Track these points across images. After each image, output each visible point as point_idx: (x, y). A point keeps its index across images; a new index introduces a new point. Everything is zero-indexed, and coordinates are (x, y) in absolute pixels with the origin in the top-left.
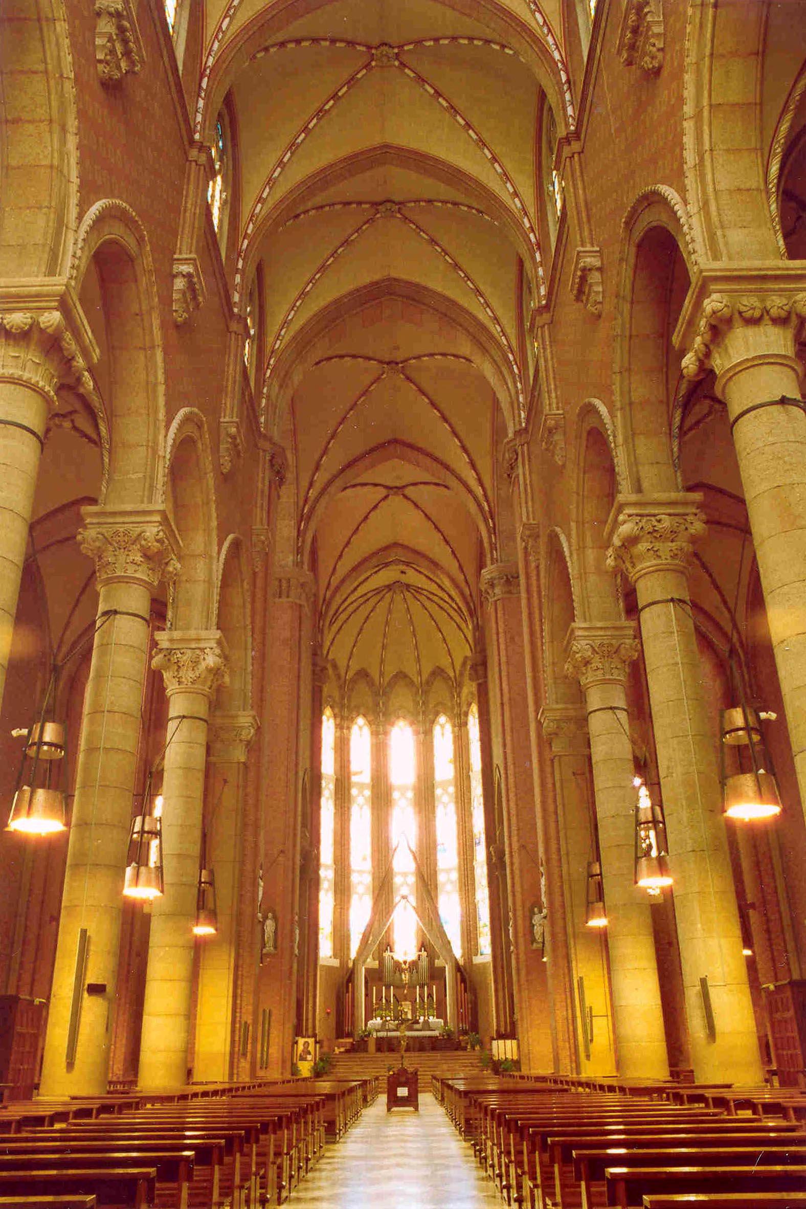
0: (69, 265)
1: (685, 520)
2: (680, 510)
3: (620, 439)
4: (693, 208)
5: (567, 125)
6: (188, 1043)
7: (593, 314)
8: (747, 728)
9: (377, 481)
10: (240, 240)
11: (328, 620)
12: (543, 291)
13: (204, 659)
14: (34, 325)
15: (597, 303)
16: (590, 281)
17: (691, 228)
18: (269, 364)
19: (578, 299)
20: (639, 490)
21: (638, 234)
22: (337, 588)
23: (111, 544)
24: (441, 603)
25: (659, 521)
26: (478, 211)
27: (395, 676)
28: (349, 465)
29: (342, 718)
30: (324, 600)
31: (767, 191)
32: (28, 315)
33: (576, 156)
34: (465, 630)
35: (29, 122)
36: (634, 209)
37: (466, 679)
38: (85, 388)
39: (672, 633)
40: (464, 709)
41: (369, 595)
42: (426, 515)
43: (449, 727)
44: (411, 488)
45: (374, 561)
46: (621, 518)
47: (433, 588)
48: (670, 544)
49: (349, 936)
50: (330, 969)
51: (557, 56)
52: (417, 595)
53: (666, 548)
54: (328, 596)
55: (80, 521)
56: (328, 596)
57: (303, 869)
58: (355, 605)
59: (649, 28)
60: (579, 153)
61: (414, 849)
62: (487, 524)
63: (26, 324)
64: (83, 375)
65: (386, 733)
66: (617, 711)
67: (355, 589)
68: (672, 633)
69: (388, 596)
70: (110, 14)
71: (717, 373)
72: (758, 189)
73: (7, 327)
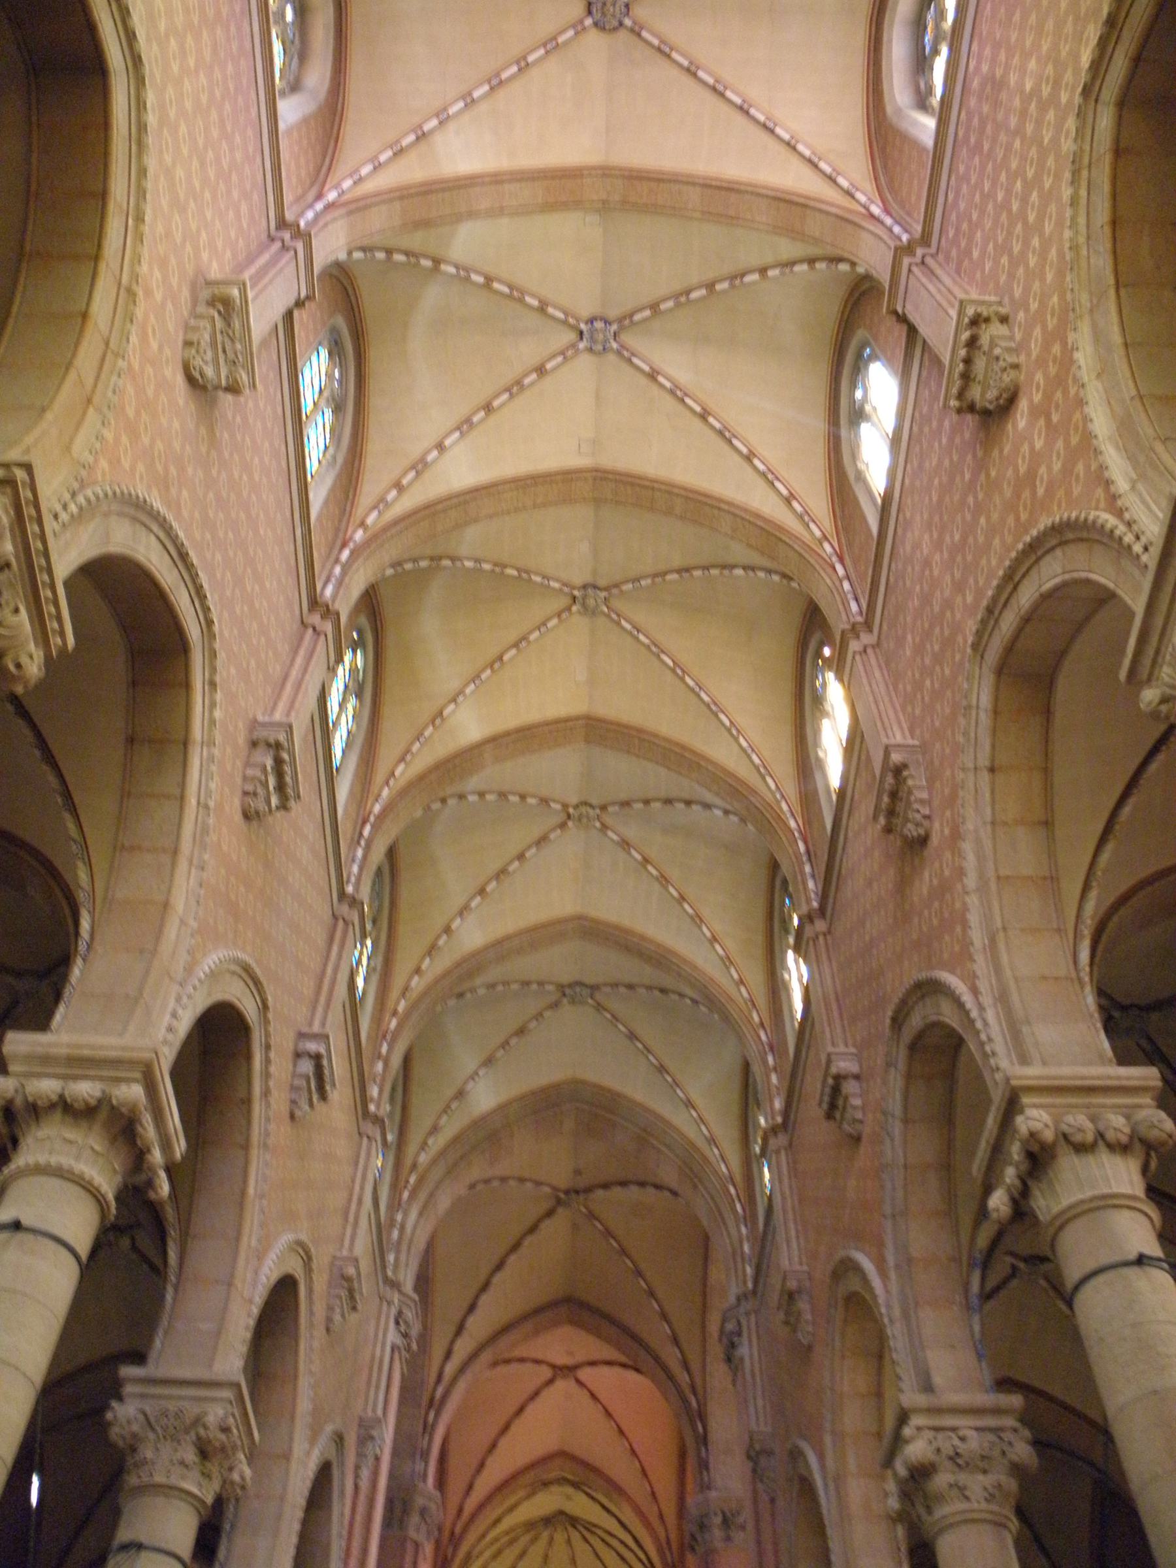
0: (165, 1024)
1: (1000, 1438)
2: (990, 1421)
3: (897, 1312)
4: (987, 1000)
5: (808, 901)
6: (342, 1454)
7: (851, 1136)
9: (540, 1356)
12: (778, 1104)
14: (104, 1101)
15: (855, 1121)
16: (844, 1091)
17: (986, 1024)
18: (407, 1182)
19: (829, 1116)
20: (928, 1387)
21: (907, 1035)
23: (153, 1429)
26: (694, 1002)
28: (506, 1329)
31: (1080, 980)
33: (821, 938)
35: (148, 851)
36: (903, 1002)
38: (156, 1193)
42: (606, 1411)
45: (530, 1477)
46: (907, 1431)
48: (981, 1477)
51: (793, 824)
52: (587, 1535)
53: (977, 1484)
54: (458, 1530)
55: (115, 1390)
56: (458, 1530)
59: (910, 792)
60: (825, 935)
62: (695, 1430)
64: (158, 1176)
70: (269, 745)
71: (1041, 1218)
72: (1067, 978)
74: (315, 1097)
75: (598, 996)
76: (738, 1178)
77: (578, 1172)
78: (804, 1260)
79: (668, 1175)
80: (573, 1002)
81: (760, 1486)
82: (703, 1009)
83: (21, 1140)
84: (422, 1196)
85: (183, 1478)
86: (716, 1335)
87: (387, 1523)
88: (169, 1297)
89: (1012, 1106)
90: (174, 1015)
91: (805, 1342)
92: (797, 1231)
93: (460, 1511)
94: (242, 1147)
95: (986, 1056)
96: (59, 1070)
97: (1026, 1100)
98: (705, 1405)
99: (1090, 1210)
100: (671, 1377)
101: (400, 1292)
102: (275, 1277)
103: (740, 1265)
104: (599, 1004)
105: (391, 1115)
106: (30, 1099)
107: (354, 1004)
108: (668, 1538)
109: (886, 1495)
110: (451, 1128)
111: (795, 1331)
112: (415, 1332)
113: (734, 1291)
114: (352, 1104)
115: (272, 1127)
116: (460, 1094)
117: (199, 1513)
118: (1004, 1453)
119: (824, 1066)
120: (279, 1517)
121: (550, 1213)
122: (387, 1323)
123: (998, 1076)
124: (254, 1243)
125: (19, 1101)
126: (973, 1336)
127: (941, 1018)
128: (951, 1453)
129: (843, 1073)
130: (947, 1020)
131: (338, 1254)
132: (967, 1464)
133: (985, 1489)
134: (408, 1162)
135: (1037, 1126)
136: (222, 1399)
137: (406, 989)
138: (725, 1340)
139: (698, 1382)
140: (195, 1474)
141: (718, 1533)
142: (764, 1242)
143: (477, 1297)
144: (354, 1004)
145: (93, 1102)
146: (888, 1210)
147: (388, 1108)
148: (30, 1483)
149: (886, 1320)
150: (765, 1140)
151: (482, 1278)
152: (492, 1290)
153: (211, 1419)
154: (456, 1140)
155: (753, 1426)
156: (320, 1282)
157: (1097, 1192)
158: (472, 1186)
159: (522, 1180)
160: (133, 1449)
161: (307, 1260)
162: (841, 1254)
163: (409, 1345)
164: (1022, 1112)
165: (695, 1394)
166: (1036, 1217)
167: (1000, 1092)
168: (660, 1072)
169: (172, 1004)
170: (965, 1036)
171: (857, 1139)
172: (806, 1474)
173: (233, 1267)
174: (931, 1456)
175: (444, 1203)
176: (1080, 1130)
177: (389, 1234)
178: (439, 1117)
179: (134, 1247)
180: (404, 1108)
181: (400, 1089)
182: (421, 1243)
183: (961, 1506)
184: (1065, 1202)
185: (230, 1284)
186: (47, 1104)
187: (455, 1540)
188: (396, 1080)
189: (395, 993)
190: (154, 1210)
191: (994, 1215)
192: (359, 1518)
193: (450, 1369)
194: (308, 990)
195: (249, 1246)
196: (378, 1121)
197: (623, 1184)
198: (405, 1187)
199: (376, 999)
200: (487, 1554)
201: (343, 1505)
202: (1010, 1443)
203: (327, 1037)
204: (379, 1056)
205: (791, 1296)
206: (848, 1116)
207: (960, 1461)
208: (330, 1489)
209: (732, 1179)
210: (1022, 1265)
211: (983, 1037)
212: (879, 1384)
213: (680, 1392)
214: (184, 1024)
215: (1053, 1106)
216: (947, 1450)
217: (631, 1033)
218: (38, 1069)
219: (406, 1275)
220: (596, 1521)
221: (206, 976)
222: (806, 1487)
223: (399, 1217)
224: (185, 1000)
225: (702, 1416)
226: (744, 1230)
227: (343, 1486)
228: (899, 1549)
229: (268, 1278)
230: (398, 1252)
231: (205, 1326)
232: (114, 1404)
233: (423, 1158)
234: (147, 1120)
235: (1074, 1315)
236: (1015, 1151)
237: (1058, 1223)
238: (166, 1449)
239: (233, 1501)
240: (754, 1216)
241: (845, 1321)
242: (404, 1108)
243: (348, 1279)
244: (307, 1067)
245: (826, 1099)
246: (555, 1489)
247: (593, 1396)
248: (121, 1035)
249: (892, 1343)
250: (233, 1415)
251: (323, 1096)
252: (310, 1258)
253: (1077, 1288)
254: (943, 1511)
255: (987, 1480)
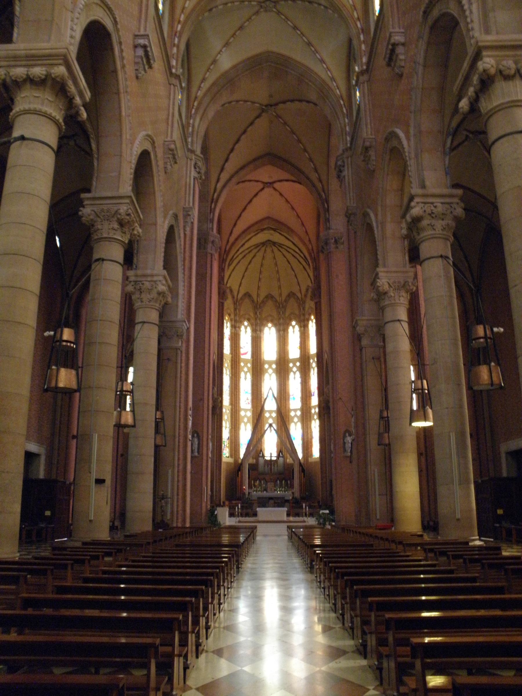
0: (68, 35)
2: (448, 200)
3: (413, 155)
7: (397, 74)
8: (485, 337)
9: (257, 179)
10: (176, 24)
11: (227, 263)
12: (364, 60)
13: (156, 287)
14: (48, 76)
17: (471, 12)
18: (193, 105)
19: (389, 65)
20: (423, 187)
22: (233, 244)
23: (99, 217)
24: (295, 254)
25: (435, 207)
26: (326, 7)
27: (267, 297)
28: (242, 168)
29: (236, 321)
30: (225, 251)
32: (44, 69)
34: (308, 270)
37: (308, 300)
38: (81, 117)
39: (440, 276)
40: (307, 317)
41: (252, 248)
43: (297, 328)
44: (278, 183)
45: (255, 228)
46: (413, 204)
47: (290, 244)
48: (441, 222)
49: (239, 445)
50: (228, 464)
53: (439, 224)
55: (81, 204)
56: (227, 249)
57: (214, 408)
58: (243, 254)
61: (276, 396)
63: (42, 75)
64: (80, 109)
65: (261, 331)
66: (402, 323)
67: (244, 244)
68: (440, 276)
69: (263, 248)
71: (482, 111)
73: (31, 76)
74: (146, 67)
75: (278, 7)
76: (345, 97)
77: (271, 96)
78: (373, 132)
79: (313, 96)
80: (266, 11)
81: (350, 227)
82: (330, 11)
83: (15, 100)
84: (201, 111)
85: (114, 234)
86: (333, 167)
87: (199, 247)
88: (96, 164)
89: (477, 56)
90: (72, 29)
91: (372, 169)
92: (370, 120)
93: (228, 241)
94: (116, 93)
95: (468, 30)
96: (24, 63)
97: (484, 53)
98: (328, 196)
99: (506, 108)
100: (314, 186)
101: (195, 155)
102: (139, 152)
103: (344, 137)
104: (279, 12)
105: (183, 74)
106: (13, 78)
107: (159, 18)
108: (312, 248)
109: (402, 228)
110: (211, 78)
111: (368, 164)
112: (203, 171)
113: (341, 147)
114: (164, 69)
115: (129, 83)
116: (214, 62)
117: (124, 247)
118: (451, 212)
119: (387, 39)
120: (156, 246)
121: (258, 117)
122: (191, 167)
123: (473, 41)
124: (128, 137)
125: (8, 80)
126: (445, 165)
127: (449, 11)
128: (430, 212)
129: (397, 43)
130: (452, 12)
131: (166, 140)
132: (436, 216)
133: (442, 226)
134: (193, 96)
135: (488, 66)
136: (125, 203)
137: (184, 8)
138: (337, 169)
139: (325, 187)
140: (119, 232)
141: (333, 246)
142: (356, 126)
143: (229, 155)
144: (159, 18)
145: (43, 77)
146: (412, 108)
147: (181, 70)
148: (56, 240)
149: (408, 158)
150: (358, 78)
151: (231, 147)
152: (235, 152)
153: (121, 211)
154: (214, 84)
155: (348, 204)
156: (160, 152)
157: (510, 99)
158: (223, 105)
159: (246, 101)
160: (93, 225)
161: (153, 143)
162: (390, 130)
163: (201, 177)
164: (481, 59)
165: (324, 191)
166: (480, 111)
167: (473, 48)
168: (308, 45)
169: (70, 23)
170: (459, 20)
171: (401, 76)
172: (369, 222)
173: (121, 148)
174: (421, 213)
175: (211, 114)
176: (509, 69)
177: (188, 129)
178: (206, 74)
179: (76, 145)
180: (189, 70)
181: (186, 61)
182: (202, 133)
183: (431, 232)
184: (495, 104)
185: (121, 156)
186: (22, 80)
187: (227, 252)
188: (183, 56)
189: (178, 11)
190: (81, 125)
191: (461, 110)
192: (187, 246)
193: (219, 185)
194: (136, 13)
195: (126, 138)
196: (177, 77)
197: (292, 101)
198: (193, 108)
199: (169, 15)
200: (240, 257)
201: (180, 241)
202: (455, 209)
203: (148, 36)
204: (174, 45)
205: (367, 149)
206: (397, 64)
207: (434, 216)
208: (174, 235)
209: (341, 96)
210: (471, 135)
211: (469, 20)
212: (403, 185)
213: (317, 190)
214: (78, 35)
215: (498, 56)
216: (428, 211)
217: (295, 27)
218: (13, 63)
219: (197, 147)
220: (283, 243)
221: (83, 5)
222: (369, 228)
223: (191, 121)
224: (76, 20)
225: (327, 201)
226: (346, 120)
227: (179, 234)
228: (405, 249)
229: (137, 151)
230: (192, 137)
231: (114, 174)
232: (81, 209)
233: (200, 94)
234: (70, 83)
235: (490, 158)
236: (475, 79)
237: (489, 115)
238: (106, 223)
239: (136, 243)
240: (351, 114)
241: (390, 159)
242: (189, 70)
243: (172, 150)
244: (140, 52)
245: (388, 56)
246: (266, 232)
247: (281, 194)
248: (49, 41)
249: (409, 168)
250: (130, 209)
251: (150, 67)
252: (154, 142)
253: (494, 143)
254: (423, 234)
255: (444, 223)
